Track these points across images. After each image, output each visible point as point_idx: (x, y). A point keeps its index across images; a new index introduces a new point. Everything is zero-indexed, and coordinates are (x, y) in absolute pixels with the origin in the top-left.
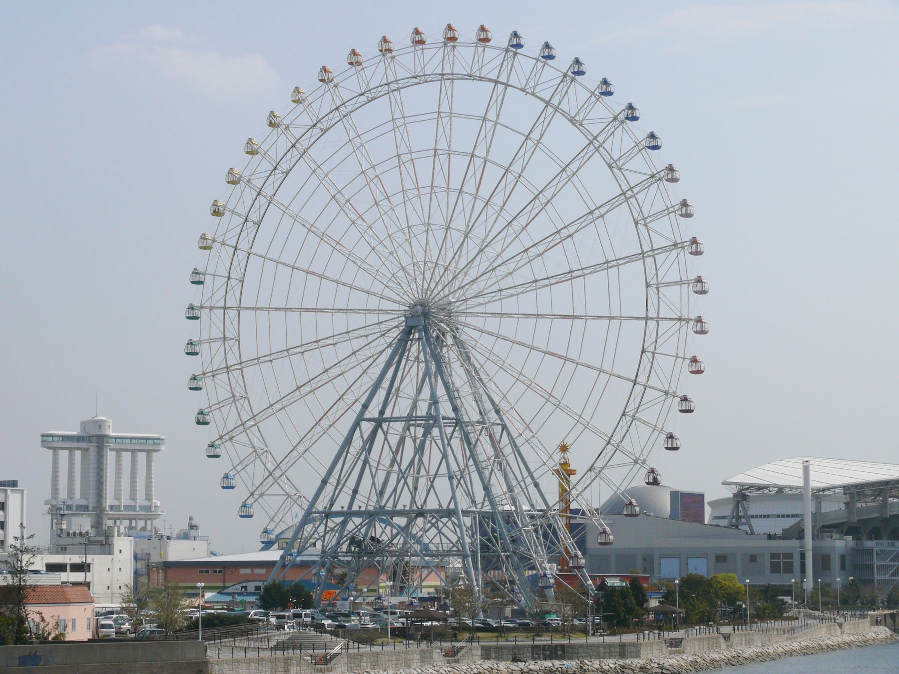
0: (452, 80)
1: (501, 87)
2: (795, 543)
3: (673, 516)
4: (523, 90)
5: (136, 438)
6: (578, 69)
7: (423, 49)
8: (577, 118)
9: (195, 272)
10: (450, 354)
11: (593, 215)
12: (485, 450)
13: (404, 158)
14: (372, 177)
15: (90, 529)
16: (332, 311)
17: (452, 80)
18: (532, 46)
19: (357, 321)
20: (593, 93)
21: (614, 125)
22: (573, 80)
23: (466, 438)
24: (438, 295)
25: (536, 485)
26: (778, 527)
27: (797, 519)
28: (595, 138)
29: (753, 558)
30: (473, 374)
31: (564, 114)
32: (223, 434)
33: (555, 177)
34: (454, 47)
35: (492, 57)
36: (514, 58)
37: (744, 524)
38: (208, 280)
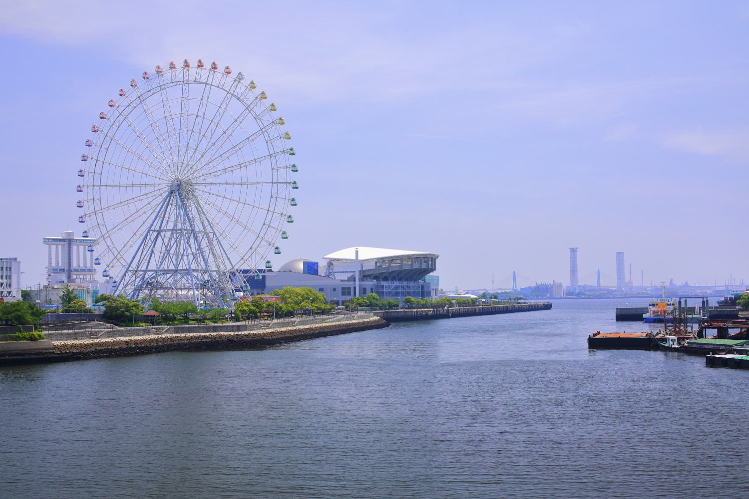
0: (188, 83)
1: (208, 86)
2: (352, 283)
3: (304, 272)
4: (218, 87)
6: (240, 77)
9: (81, 171)
10: (190, 203)
12: (204, 244)
13: (168, 118)
14: (155, 127)
17: (188, 83)
18: (221, 69)
19: (149, 189)
20: (247, 87)
22: (239, 82)
23: (196, 238)
24: (183, 177)
25: (228, 259)
26: (345, 277)
27: (353, 273)
28: (249, 106)
29: (334, 290)
30: (200, 211)
31: (235, 96)
34: (188, 70)
35: (204, 74)
37: (331, 275)
38: (86, 174)
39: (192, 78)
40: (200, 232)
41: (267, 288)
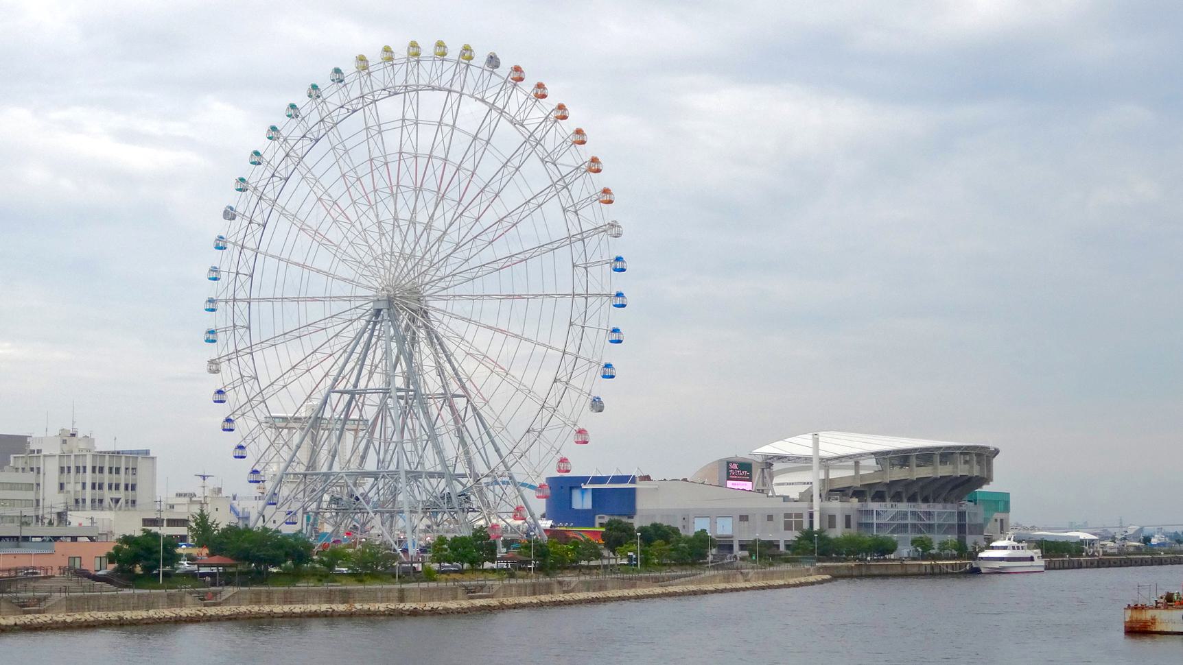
2: (805, 505)
5: (277, 418)
7: (393, 65)
8: (518, 118)
11: (533, 203)
15: (211, 487)
16: (323, 299)
21: (522, 114)
27: (807, 487)
29: (770, 518)
32: (235, 409)
33: (498, 172)
36: (467, 70)
38: (223, 276)
39: (423, 81)
40: (434, 396)
41: (638, 513)
